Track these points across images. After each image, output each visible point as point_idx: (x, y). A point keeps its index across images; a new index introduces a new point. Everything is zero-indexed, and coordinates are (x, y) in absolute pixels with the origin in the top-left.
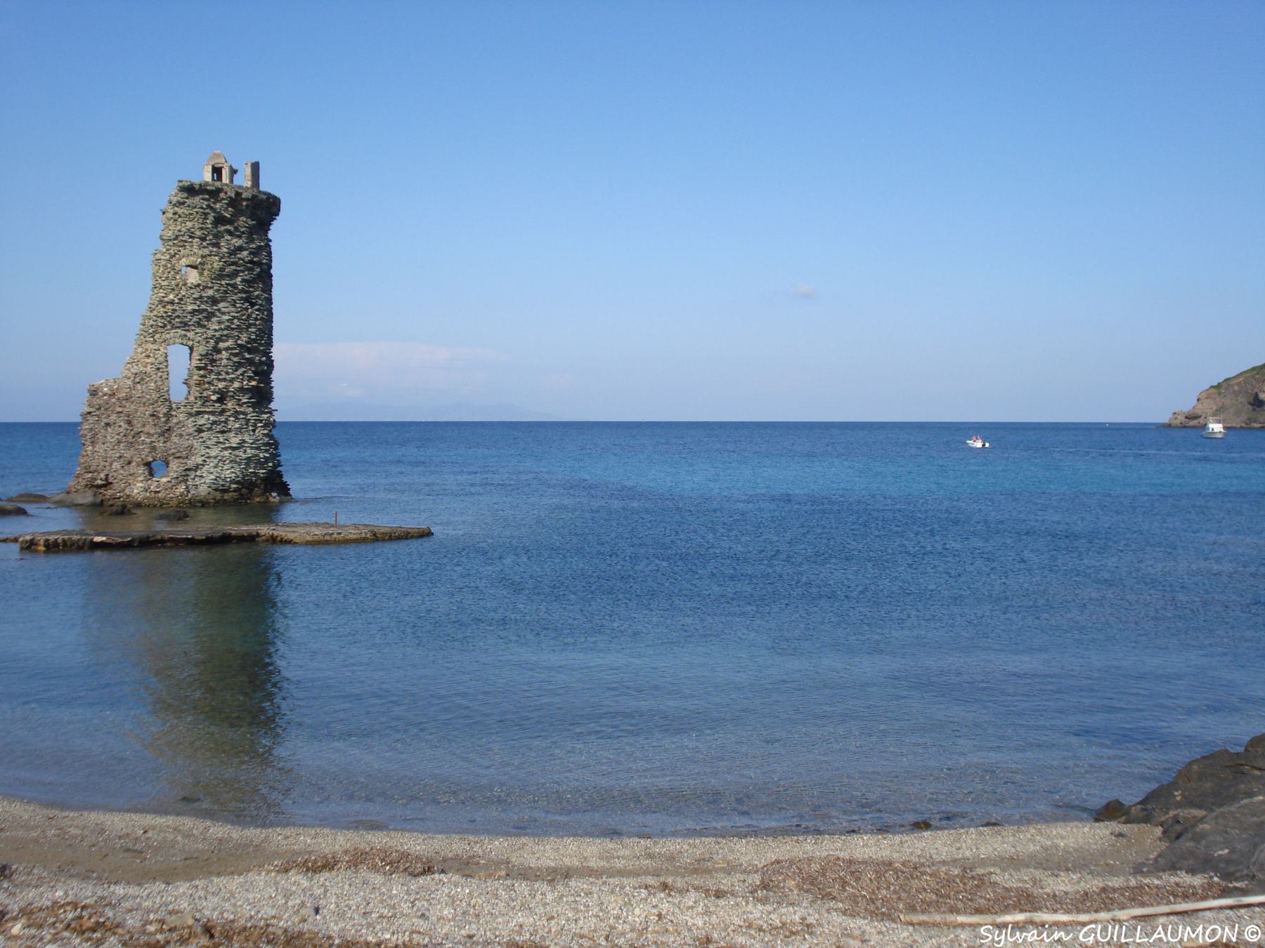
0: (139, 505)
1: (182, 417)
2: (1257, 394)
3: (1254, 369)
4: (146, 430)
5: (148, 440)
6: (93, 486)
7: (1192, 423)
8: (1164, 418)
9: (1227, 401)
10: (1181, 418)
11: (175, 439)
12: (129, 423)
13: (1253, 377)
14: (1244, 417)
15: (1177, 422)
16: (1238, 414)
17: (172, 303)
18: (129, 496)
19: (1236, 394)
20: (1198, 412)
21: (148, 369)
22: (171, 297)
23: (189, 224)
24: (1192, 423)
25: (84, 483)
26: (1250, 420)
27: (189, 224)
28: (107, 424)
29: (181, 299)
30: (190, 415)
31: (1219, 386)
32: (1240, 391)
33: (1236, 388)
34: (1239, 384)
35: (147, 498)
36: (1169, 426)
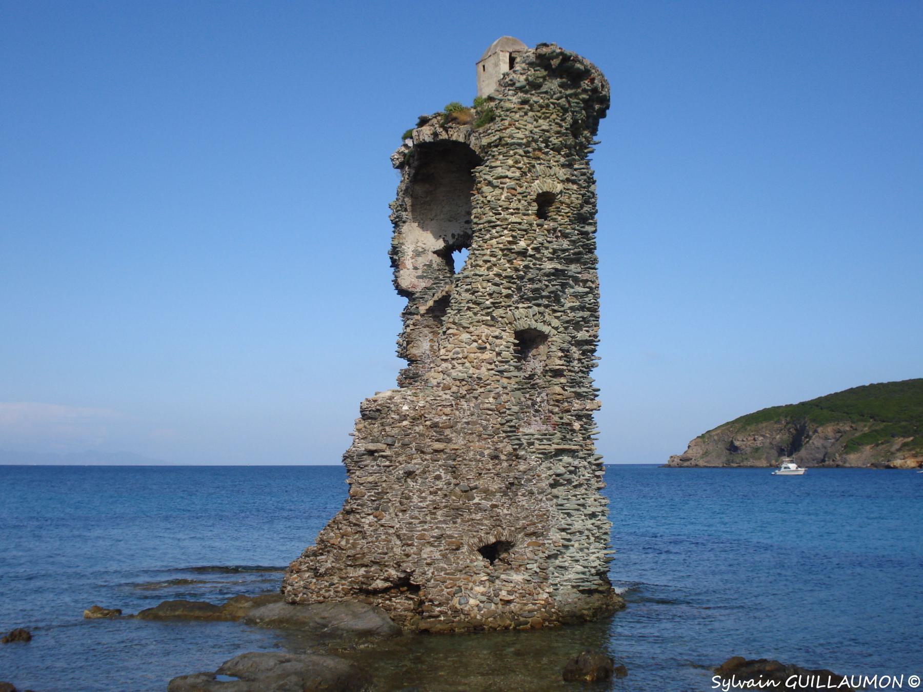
0: (476, 629)
1: (533, 459)
2: (732, 442)
3: (728, 423)
4: (480, 483)
5: (487, 504)
6: (368, 593)
7: (686, 464)
8: (665, 461)
9: (711, 448)
10: (677, 461)
11: (523, 501)
12: (454, 471)
13: (728, 429)
14: (724, 459)
15: (675, 463)
16: (719, 457)
17: (523, 254)
18: (456, 612)
19: (716, 442)
20: (689, 455)
21: (483, 372)
22: (522, 244)
23: (544, 124)
24: (686, 464)
25: (346, 585)
26: (729, 462)
27: (544, 124)
28: (409, 474)
29: (536, 249)
30: (547, 456)
31: (703, 436)
32: (719, 440)
33: (716, 438)
34: (717, 435)
35: (493, 614)
36: (669, 466)
